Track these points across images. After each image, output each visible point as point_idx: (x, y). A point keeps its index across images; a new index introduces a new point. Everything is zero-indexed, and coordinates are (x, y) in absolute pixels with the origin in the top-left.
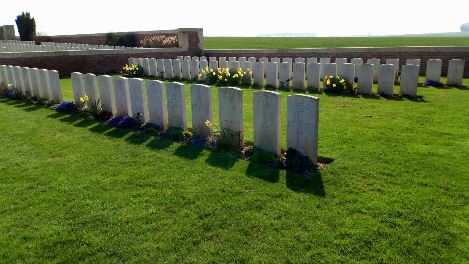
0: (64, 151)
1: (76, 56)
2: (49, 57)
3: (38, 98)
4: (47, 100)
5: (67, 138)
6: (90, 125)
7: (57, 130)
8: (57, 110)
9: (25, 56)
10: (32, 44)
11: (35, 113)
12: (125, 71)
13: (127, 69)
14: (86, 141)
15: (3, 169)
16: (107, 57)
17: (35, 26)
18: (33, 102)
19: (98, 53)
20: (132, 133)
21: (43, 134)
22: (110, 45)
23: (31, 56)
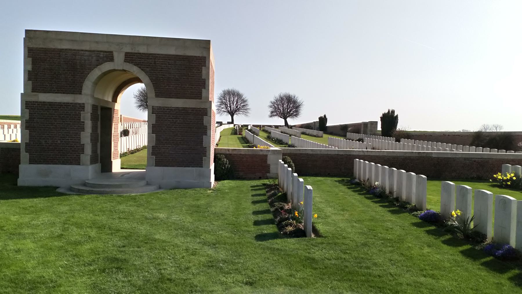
0: (436, 272)
1: (438, 158)
2: (410, 157)
3: (400, 199)
4: (409, 204)
5: (435, 255)
6: (461, 246)
7: (424, 242)
8: (421, 218)
9: (390, 155)
10: (391, 141)
11: (399, 217)
12: (495, 180)
13: (500, 177)
14: (459, 266)
15: (378, 276)
16: (475, 161)
17: (397, 122)
18: (395, 203)
19: (464, 156)
20: (517, 271)
21: (410, 245)
22: (477, 146)
23: (395, 155)
